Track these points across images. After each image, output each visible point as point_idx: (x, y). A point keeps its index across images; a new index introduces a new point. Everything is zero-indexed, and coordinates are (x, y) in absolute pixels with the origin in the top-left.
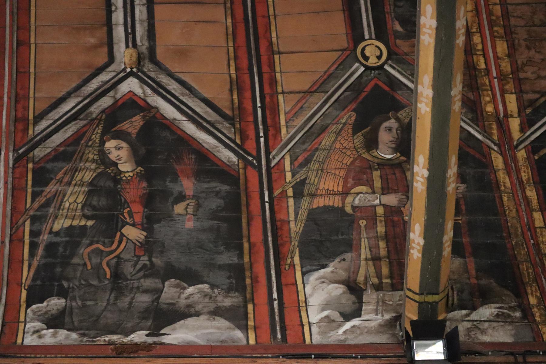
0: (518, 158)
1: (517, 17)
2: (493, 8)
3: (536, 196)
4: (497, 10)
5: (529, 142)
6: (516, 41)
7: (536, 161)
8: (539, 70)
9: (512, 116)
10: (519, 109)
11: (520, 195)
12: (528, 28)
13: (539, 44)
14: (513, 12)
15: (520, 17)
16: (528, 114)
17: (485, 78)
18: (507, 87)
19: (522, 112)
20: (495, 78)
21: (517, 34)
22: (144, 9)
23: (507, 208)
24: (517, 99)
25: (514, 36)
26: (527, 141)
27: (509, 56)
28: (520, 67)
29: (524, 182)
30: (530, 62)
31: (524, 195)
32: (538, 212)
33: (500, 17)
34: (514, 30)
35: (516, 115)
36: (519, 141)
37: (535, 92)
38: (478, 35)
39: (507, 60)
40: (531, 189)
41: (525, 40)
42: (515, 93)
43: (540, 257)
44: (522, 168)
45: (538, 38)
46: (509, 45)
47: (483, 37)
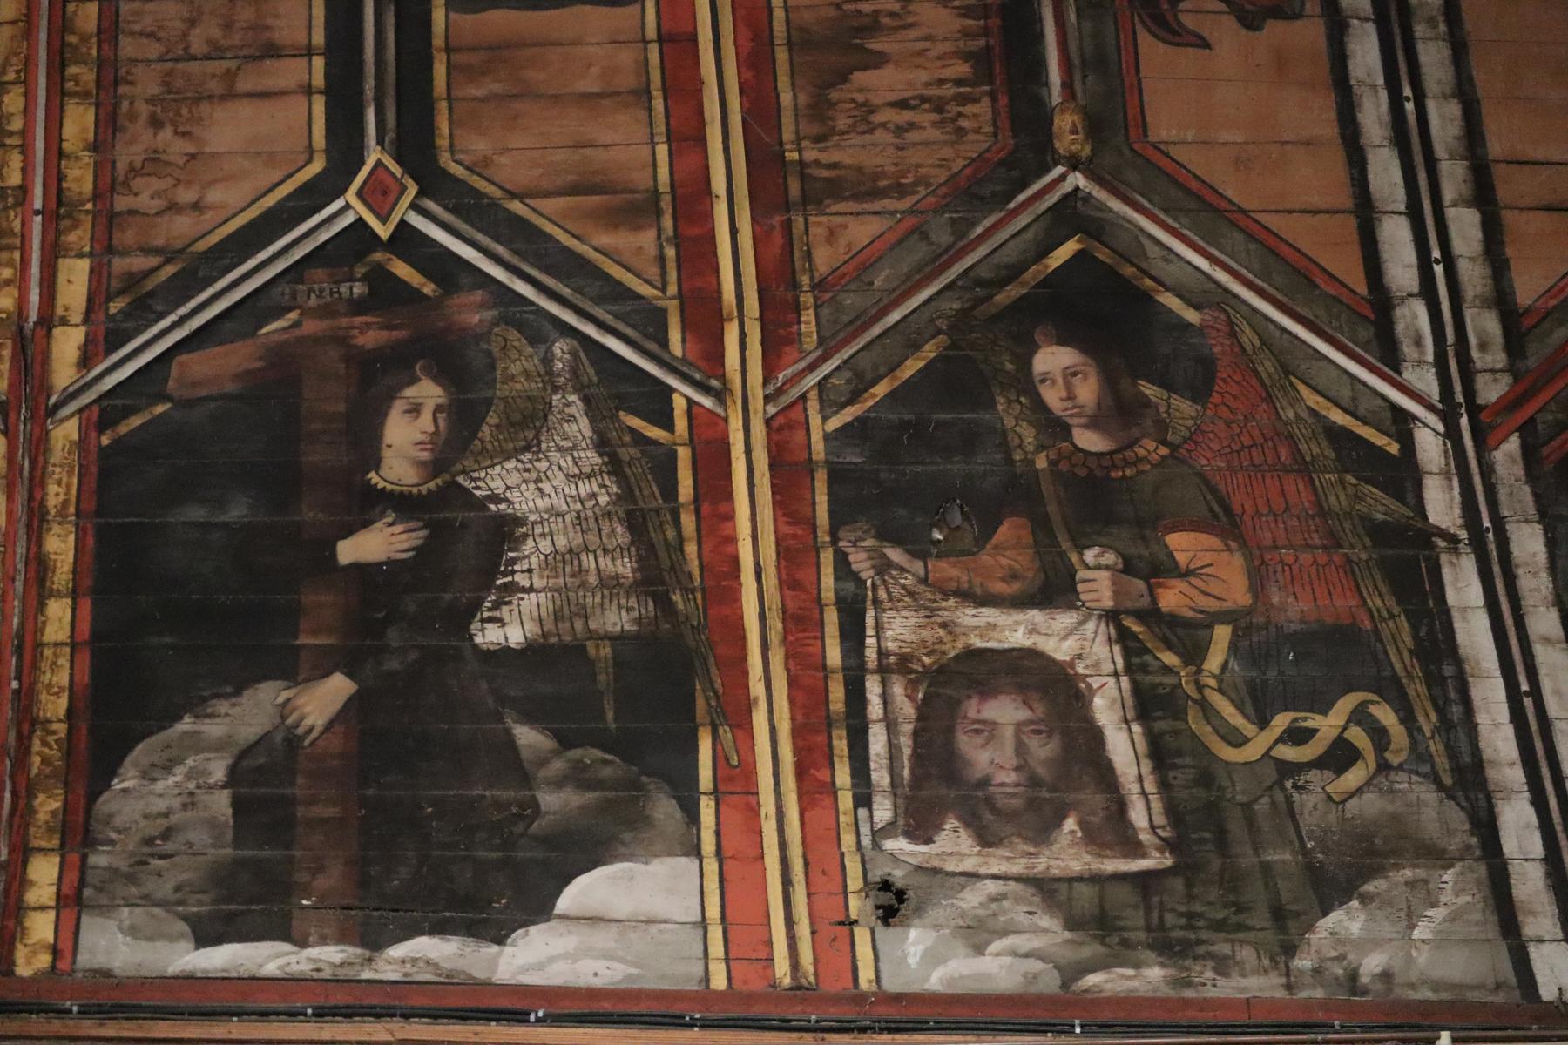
0: (52, 442)
1: (141, 34)
2: (75, 13)
3: (72, 553)
4: (87, 17)
5: (94, 396)
6: (125, 105)
7: (102, 450)
8: (175, 186)
9: (64, 322)
10: (90, 300)
11: (19, 550)
12: (169, 65)
13: (190, 111)
14: (129, 22)
15: (151, 35)
16: (114, 315)
17: (12, 214)
18: (72, 238)
19: (96, 308)
20: (37, 213)
21: (132, 83)
22: (1454, 109)
23: (579, 624)
24: (92, 271)
25: (122, 89)
26: (88, 394)
27: (94, 147)
28: (121, 178)
29: (48, 513)
30: (155, 162)
31: (34, 549)
32: (64, 600)
33: (91, 37)
34: (128, 73)
35: (76, 317)
36: (65, 394)
37: (147, 251)
38: (20, 89)
39: (87, 160)
40: (62, 533)
41: (151, 101)
42: (91, 254)
43: (26, 728)
44: (54, 472)
45: (189, 95)
46: (101, 117)
47: (29, 96)
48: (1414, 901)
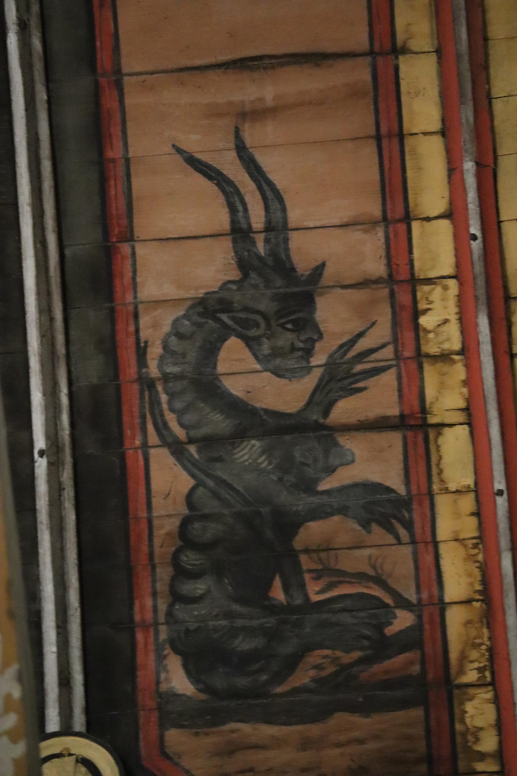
38: (487, 694)
48: (438, 283)
